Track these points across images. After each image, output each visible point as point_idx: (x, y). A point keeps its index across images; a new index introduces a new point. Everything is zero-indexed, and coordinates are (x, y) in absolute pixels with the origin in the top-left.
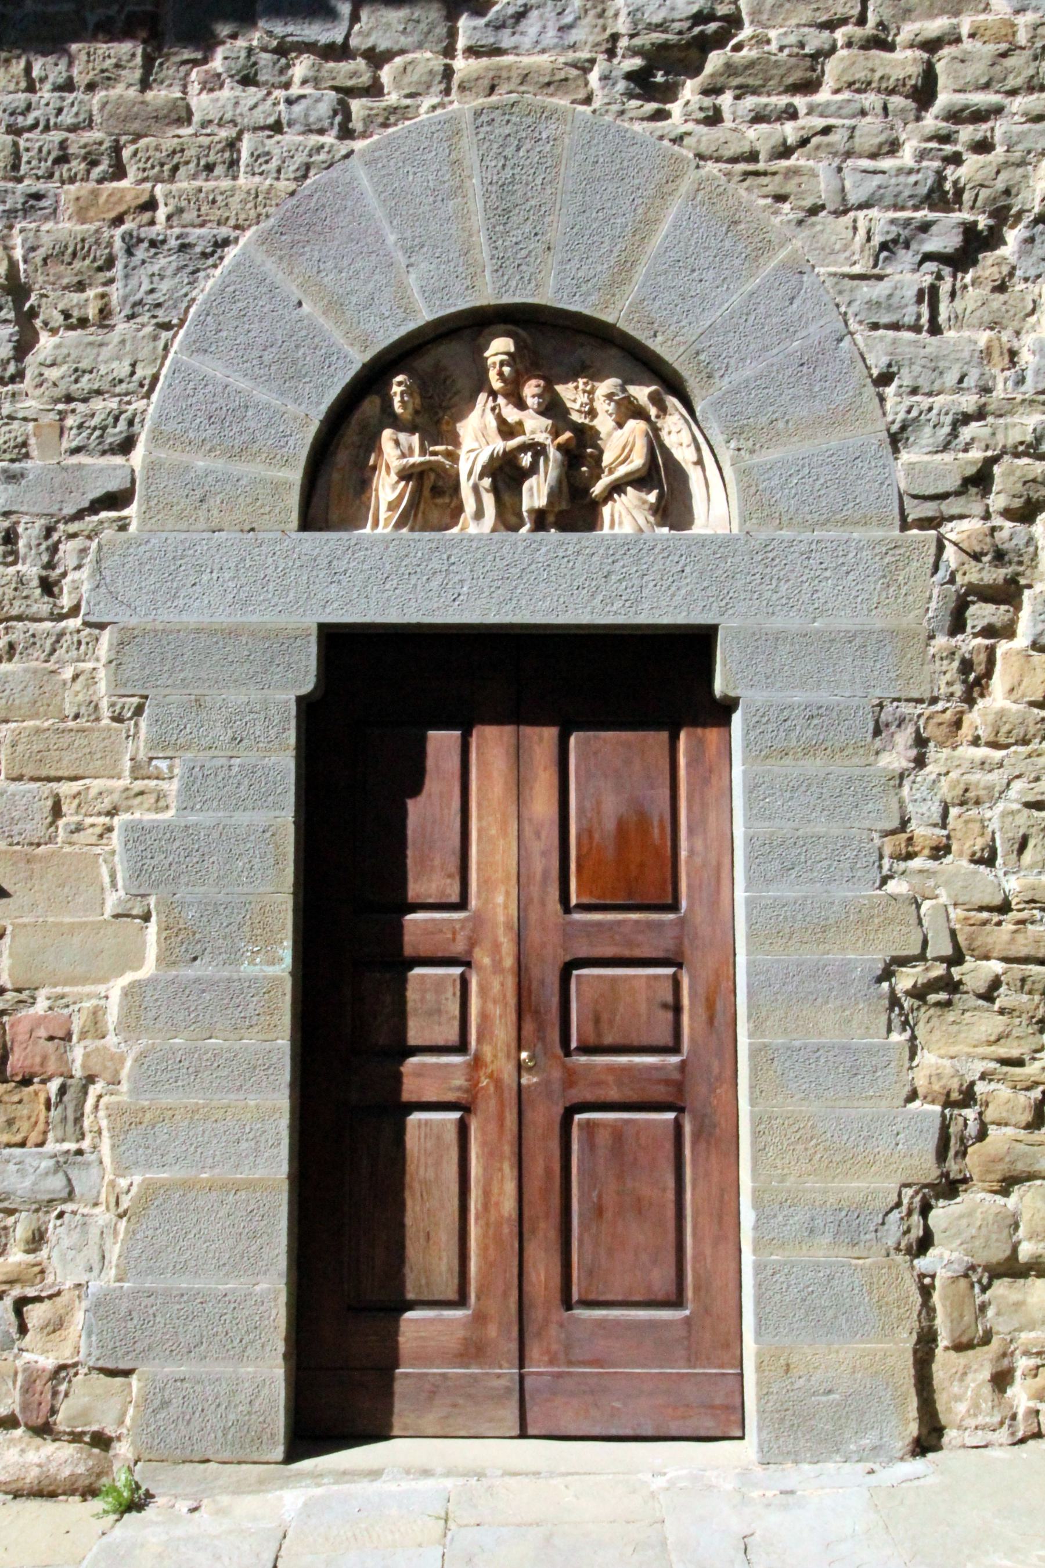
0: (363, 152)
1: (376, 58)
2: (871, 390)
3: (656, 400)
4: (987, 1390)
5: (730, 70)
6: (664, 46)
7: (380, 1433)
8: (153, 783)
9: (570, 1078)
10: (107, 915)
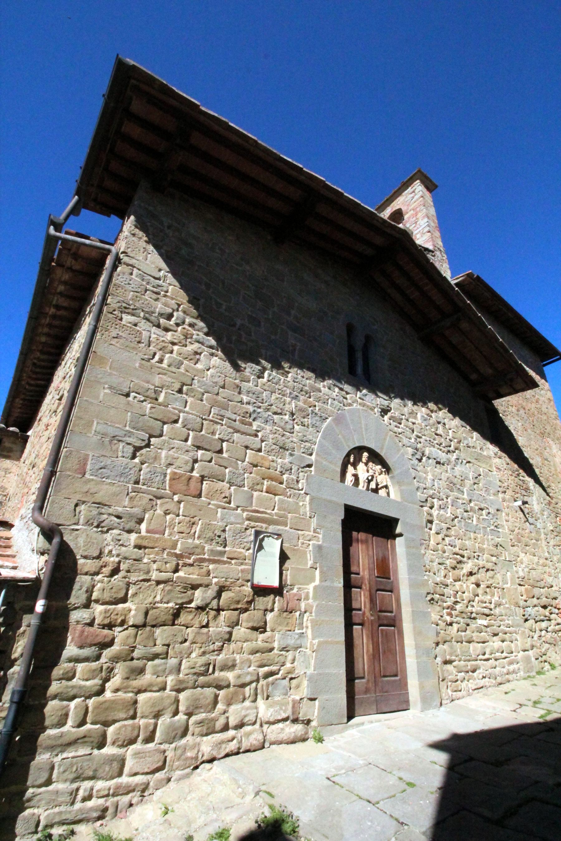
10: (309, 566)
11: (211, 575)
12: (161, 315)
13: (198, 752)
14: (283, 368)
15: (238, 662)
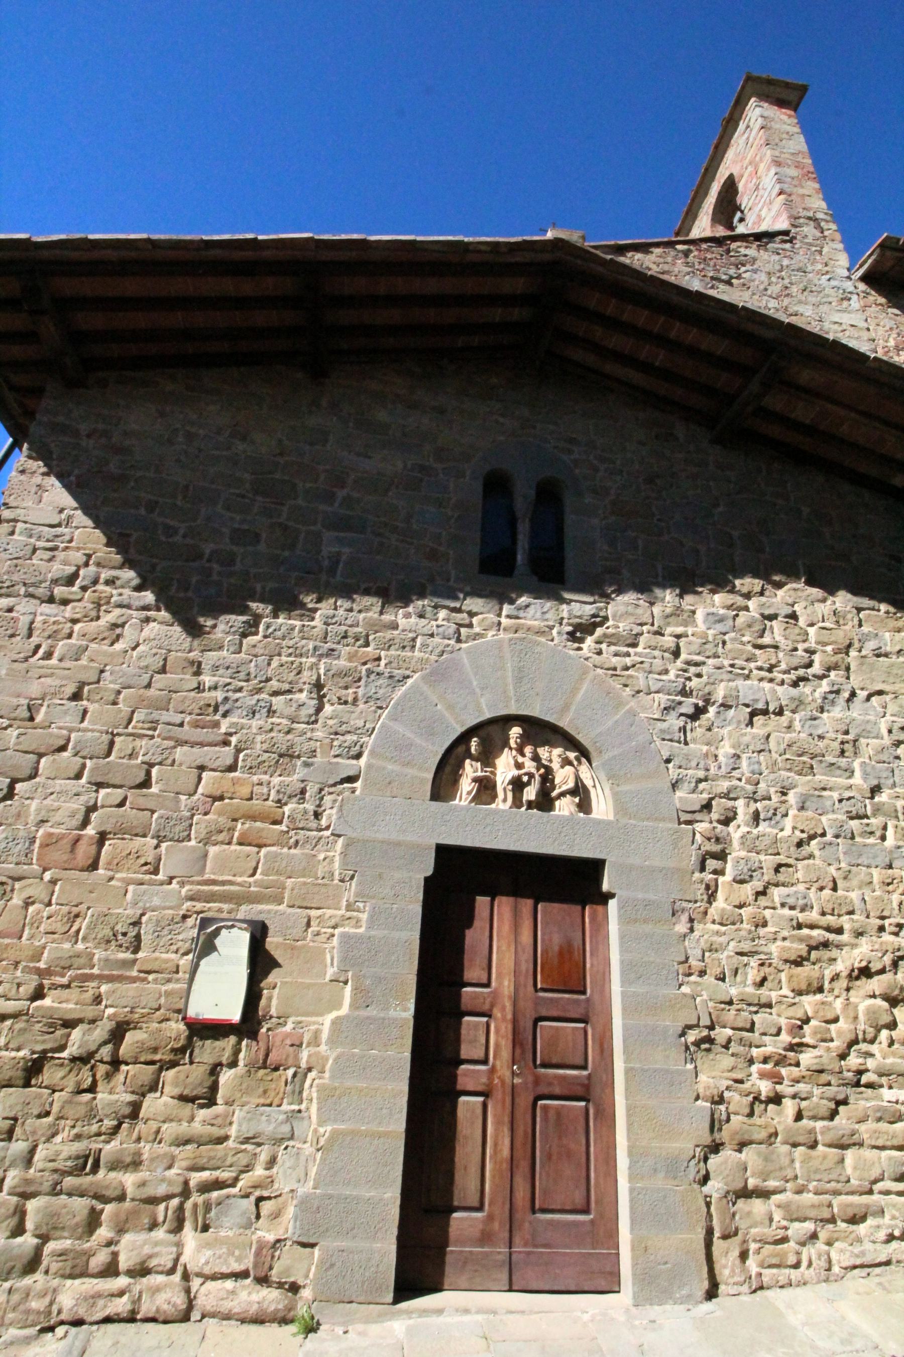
0: (465, 649)
1: (471, 614)
2: (663, 765)
3: (577, 758)
4: (738, 1261)
5: (605, 635)
6: (580, 624)
7: (436, 1288)
8: (355, 914)
9: (537, 1081)
10: (328, 978)
11: (104, 1003)
12: (55, 582)
13: (51, 1303)
14: (303, 606)
15: (145, 1157)
